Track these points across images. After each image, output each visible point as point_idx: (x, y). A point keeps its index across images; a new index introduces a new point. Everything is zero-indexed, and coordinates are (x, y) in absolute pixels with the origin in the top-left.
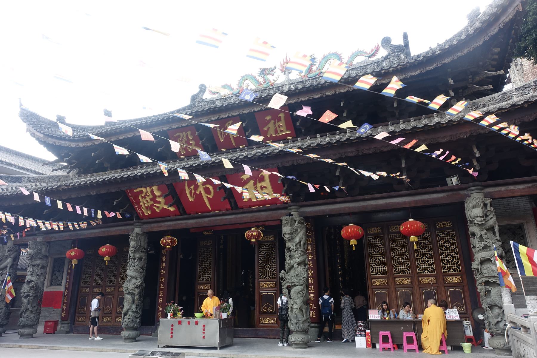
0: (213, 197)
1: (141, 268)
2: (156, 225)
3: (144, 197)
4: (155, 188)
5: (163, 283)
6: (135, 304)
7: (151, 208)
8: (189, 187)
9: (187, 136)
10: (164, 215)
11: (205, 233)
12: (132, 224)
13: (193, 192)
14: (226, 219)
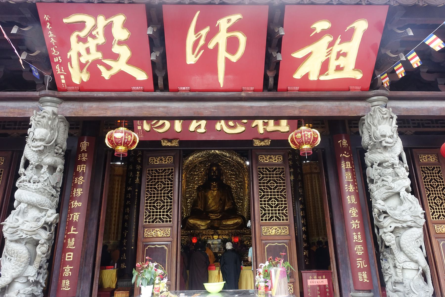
0: (239, 61)
1: (54, 187)
2: (94, 105)
3: (83, 40)
4: (119, 20)
5: (76, 224)
6: (36, 264)
7: (93, 68)
8: (197, 30)
9: (108, 29)
10: (121, 88)
11: (164, 144)
12: (35, 99)
13: (202, 42)
14: (251, 107)
